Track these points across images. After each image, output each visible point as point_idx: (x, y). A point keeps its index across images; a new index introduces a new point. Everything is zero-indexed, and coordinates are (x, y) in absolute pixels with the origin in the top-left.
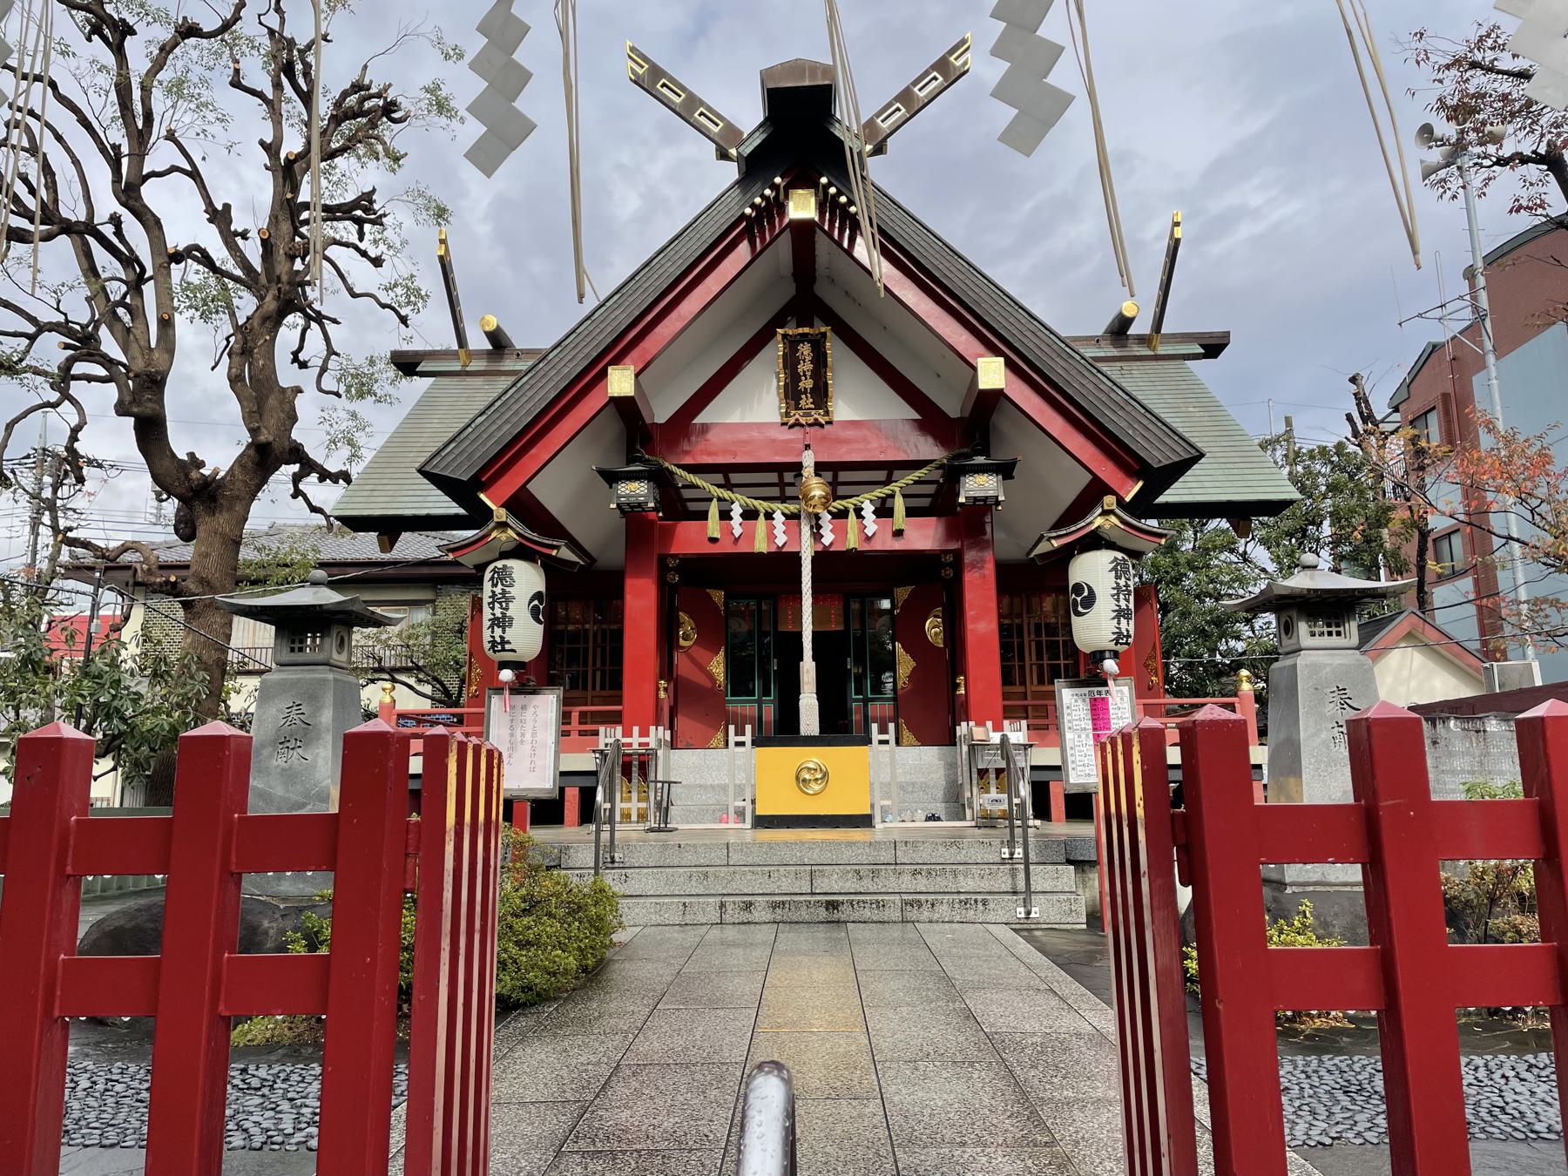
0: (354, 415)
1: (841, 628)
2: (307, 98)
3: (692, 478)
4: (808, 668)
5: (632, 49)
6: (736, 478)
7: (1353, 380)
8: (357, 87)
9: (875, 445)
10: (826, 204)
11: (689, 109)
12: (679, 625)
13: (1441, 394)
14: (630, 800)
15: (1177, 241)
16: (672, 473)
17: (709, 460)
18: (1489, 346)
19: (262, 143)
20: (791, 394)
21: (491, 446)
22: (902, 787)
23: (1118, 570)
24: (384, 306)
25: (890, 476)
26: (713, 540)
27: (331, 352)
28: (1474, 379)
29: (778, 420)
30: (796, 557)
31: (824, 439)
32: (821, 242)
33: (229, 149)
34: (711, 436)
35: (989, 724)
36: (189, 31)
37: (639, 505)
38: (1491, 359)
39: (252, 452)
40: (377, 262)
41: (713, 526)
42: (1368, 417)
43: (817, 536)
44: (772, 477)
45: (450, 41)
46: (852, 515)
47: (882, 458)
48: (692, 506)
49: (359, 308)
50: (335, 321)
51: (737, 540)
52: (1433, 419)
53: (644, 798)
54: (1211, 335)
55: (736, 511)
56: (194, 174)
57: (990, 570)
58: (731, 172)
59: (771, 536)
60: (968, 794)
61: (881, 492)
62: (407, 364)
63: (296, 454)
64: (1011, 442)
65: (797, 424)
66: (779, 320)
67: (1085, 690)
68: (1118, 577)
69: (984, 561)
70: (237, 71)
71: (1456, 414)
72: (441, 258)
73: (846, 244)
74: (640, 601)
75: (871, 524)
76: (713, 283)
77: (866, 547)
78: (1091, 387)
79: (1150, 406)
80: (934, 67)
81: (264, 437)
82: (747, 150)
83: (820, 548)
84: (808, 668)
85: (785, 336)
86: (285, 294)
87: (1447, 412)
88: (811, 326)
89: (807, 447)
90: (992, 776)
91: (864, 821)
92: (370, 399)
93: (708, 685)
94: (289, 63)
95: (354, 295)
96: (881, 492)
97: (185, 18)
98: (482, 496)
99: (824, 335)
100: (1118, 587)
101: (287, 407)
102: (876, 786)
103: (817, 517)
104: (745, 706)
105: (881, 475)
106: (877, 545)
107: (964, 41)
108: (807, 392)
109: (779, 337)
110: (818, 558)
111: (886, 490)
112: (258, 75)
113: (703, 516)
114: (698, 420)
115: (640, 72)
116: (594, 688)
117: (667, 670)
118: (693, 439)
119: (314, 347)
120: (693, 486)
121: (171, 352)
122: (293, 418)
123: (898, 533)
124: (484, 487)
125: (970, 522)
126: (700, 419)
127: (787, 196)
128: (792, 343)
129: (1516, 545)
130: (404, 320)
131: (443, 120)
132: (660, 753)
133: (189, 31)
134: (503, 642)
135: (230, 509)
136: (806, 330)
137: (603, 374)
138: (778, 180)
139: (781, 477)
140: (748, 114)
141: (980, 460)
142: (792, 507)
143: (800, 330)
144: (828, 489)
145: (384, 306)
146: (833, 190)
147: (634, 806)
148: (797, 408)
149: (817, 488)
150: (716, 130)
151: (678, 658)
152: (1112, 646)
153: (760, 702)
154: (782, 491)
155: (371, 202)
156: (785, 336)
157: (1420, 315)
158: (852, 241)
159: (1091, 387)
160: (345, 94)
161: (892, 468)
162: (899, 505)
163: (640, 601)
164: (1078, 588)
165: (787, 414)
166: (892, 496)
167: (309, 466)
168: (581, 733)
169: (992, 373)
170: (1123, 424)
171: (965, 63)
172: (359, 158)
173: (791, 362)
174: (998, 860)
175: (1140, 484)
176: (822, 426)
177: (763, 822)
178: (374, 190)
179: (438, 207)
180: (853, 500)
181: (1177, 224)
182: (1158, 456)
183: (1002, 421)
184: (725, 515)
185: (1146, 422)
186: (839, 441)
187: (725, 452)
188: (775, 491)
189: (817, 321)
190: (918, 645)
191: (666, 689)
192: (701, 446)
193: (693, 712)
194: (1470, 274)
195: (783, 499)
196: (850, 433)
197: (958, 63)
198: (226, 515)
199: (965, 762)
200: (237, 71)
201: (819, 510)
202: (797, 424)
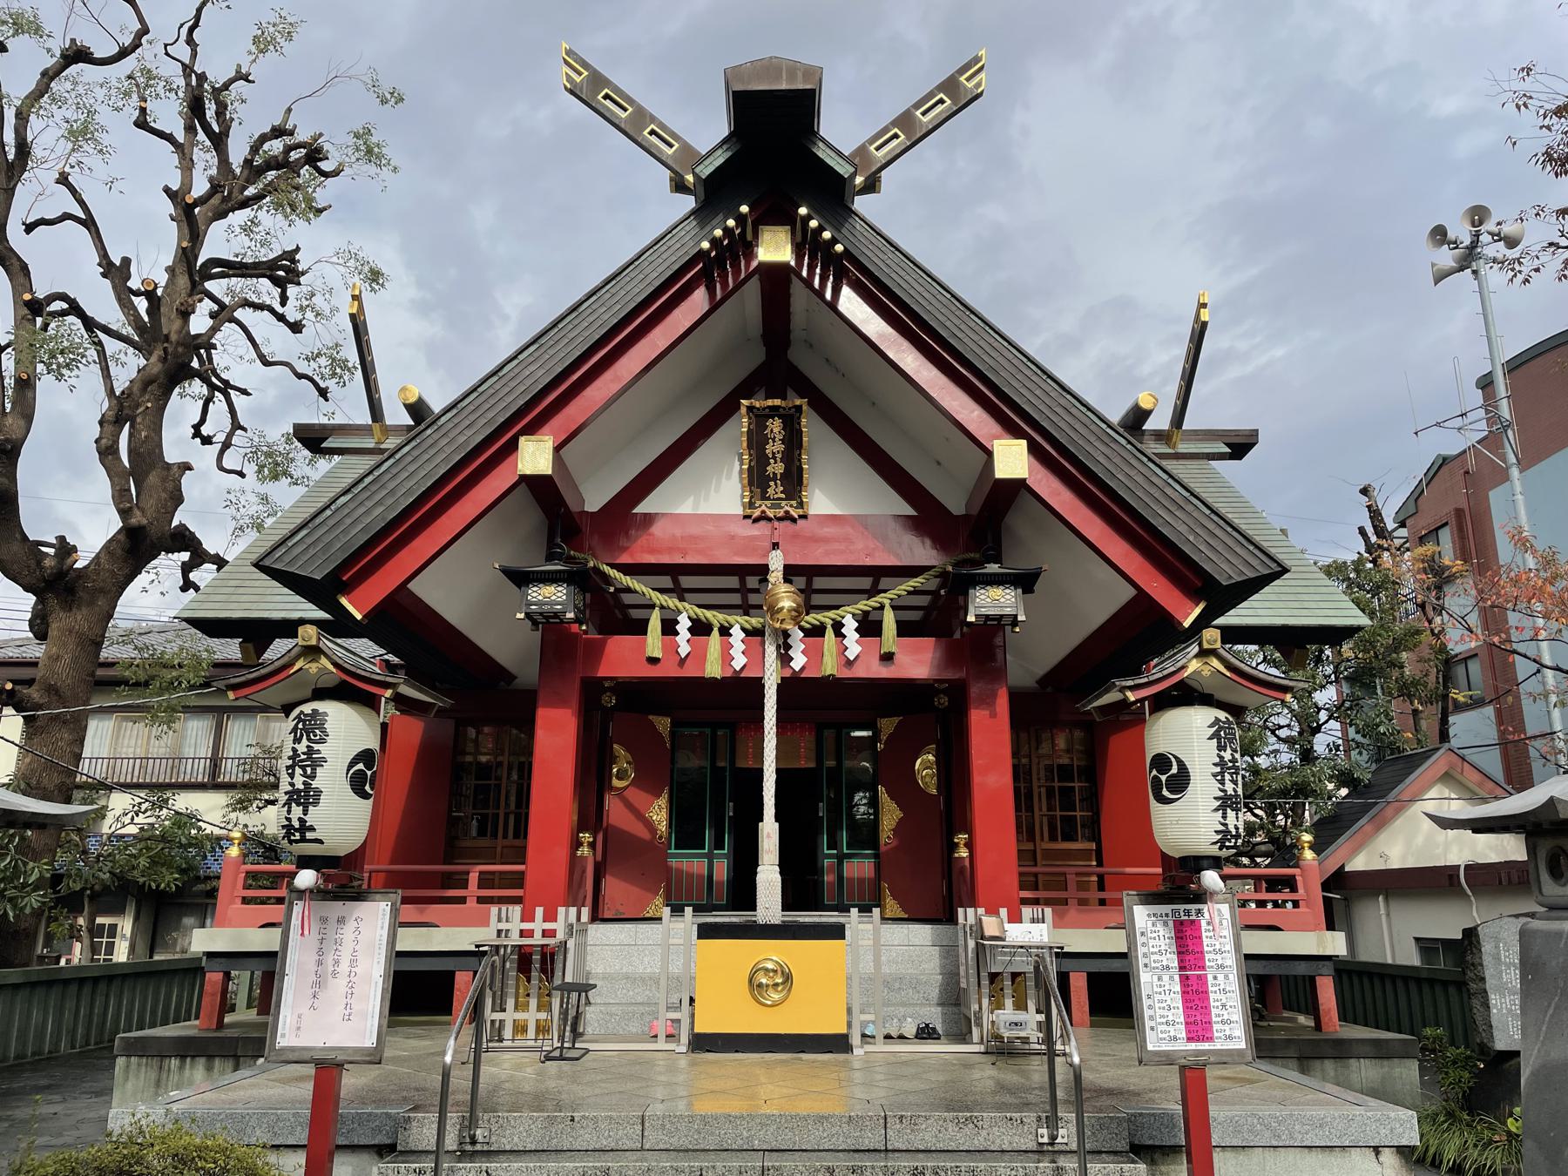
0: (265, 499)
1: (812, 765)
2: (219, 142)
3: (627, 581)
4: (769, 830)
5: (569, 52)
6: (687, 581)
7: (1365, 491)
8: (278, 132)
9: (860, 545)
10: (806, 243)
11: (636, 127)
12: (613, 759)
13: (1453, 506)
14: (526, 1007)
15: (1204, 325)
16: (607, 579)
17: (651, 559)
18: (1512, 459)
19: (167, 190)
20: (757, 480)
21: (357, 535)
22: (886, 984)
23: (1220, 736)
24: (300, 376)
25: (876, 583)
26: (653, 661)
27: (236, 425)
28: (1491, 494)
29: (739, 511)
30: (757, 685)
31: (795, 536)
32: (797, 288)
33: (110, 184)
34: (657, 529)
35: (1003, 912)
36: (77, 55)
37: (556, 615)
38: (1515, 472)
39: (122, 537)
40: (296, 327)
41: (654, 642)
42: (1381, 532)
43: (785, 659)
44: (733, 582)
45: (385, 89)
46: (830, 633)
47: (869, 562)
48: (636, 614)
49: (262, 373)
50: (245, 392)
51: (682, 662)
52: (1446, 536)
53: (544, 1006)
54: (1236, 433)
55: (684, 624)
56: (89, 223)
57: (1002, 703)
58: (689, 203)
59: (727, 658)
60: (975, 1007)
61: (864, 605)
62: (313, 439)
63: (184, 540)
64: (1028, 544)
65: (763, 517)
66: (746, 388)
67: (1167, 909)
68: (1221, 748)
69: (994, 696)
70: (143, 110)
71: (1472, 531)
72: (352, 316)
73: (828, 296)
74: (556, 736)
75: (854, 647)
76: (659, 338)
77: (846, 674)
78: (1139, 479)
79: (1216, 506)
80: (942, 87)
81: (137, 519)
82: (706, 170)
83: (788, 674)
84: (769, 830)
85: (750, 409)
86: (177, 360)
87: (1461, 528)
88: (784, 398)
89: (775, 546)
90: (1008, 983)
91: (837, 1044)
92: (285, 481)
93: (645, 834)
94: (204, 106)
95: (266, 363)
96: (864, 605)
97: (73, 41)
98: (344, 601)
99: (799, 409)
100: (1221, 763)
101: (170, 486)
102: (855, 983)
103: (786, 634)
104: (690, 863)
105: (865, 583)
106: (860, 672)
107: (977, 59)
108: (776, 479)
109: (743, 410)
110: (785, 687)
111: (873, 602)
112: (169, 114)
113: (641, 628)
114: (640, 509)
115: (578, 79)
116: (505, 836)
117: (590, 815)
118: (633, 532)
119: (217, 423)
120: (629, 590)
121: (28, 418)
122: (177, 499)
123: (887, 658)
124: (347, 588)
125: (982, 646)
126: (642, 508)
127: (756, 235)
128: (760, 418)
129: (1549, 674)
130: (323, 393)
131: (372, 169)
132: (571, 944)
133: (77, 55)
134: (304, 827)
135: (91, 603)
136: (777, 402)
137: (512, 446)
138: (744, 209)
139: (743, 582)
140: (707, 130)
141: (993, 568)
142: (755, 622)
143: (770, 402)
144: (800, 600)
145: (300, 376)
146: (814, 224)
147: (532, 1016)
148: (764, 498)
149: (786, 598)
150: (670, 151)
151: (612, 804)
152: (1214, 850)
153: (710, 857)
154: (745, 599)
155: (293, 261)
156: (750, 409)
157: (1438, 424)
158: (836, 291)
159: (1139, 479)
160: (264, 138)
161: (878, 575)
162: (889, 620)
163: (556, 736)
164: (1161, 762)
165: (751, 505)
166: (882, 607)
167: (200, 556)
168: (481, 900)
169: (1012, 459)
170: (1182, 528)
171: (979, 85)
172: (286, 217)
173: (757, 441)
174: (1032, 1145)
175: (1201, 606)
176: (794, 520)
177: (704, 1043)
178: (298, 249)
179: (372, 270)
180: (832, 614)
181: (1204, 306)
182: (1227, 571)
183: (1018, 521)
184: (669, 628)
185: (1211, 526)
186: (815, 540)
187: (671, 550)
188: (735, 599)
189: (790, 393)
190: (906, 790)
191: (592, 845)
192: (642, 541)
193: (613, 875)
194: (1486, 383)
195: (746, 609)
196: (829, 531)
197: (970, 85)
198: (84, 611)
199: (972, 962)
200: (143, 110)
201: (788, 626)
202: (763, 517)
